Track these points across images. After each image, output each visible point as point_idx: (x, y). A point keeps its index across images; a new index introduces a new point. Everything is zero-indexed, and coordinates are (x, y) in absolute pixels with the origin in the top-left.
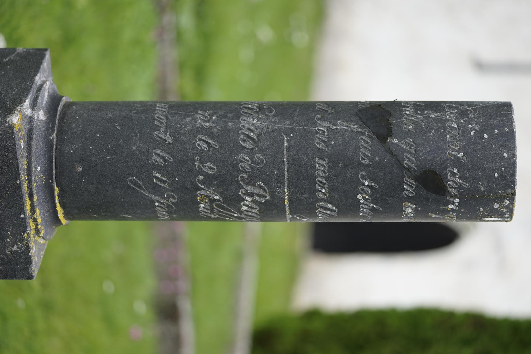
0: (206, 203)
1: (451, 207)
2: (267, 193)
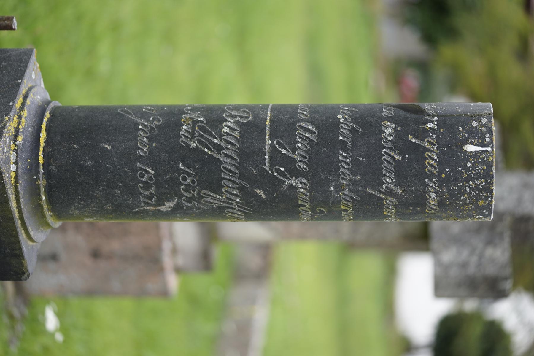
0: (189, 124)
1: (430, 125)
2: (249, 115)
